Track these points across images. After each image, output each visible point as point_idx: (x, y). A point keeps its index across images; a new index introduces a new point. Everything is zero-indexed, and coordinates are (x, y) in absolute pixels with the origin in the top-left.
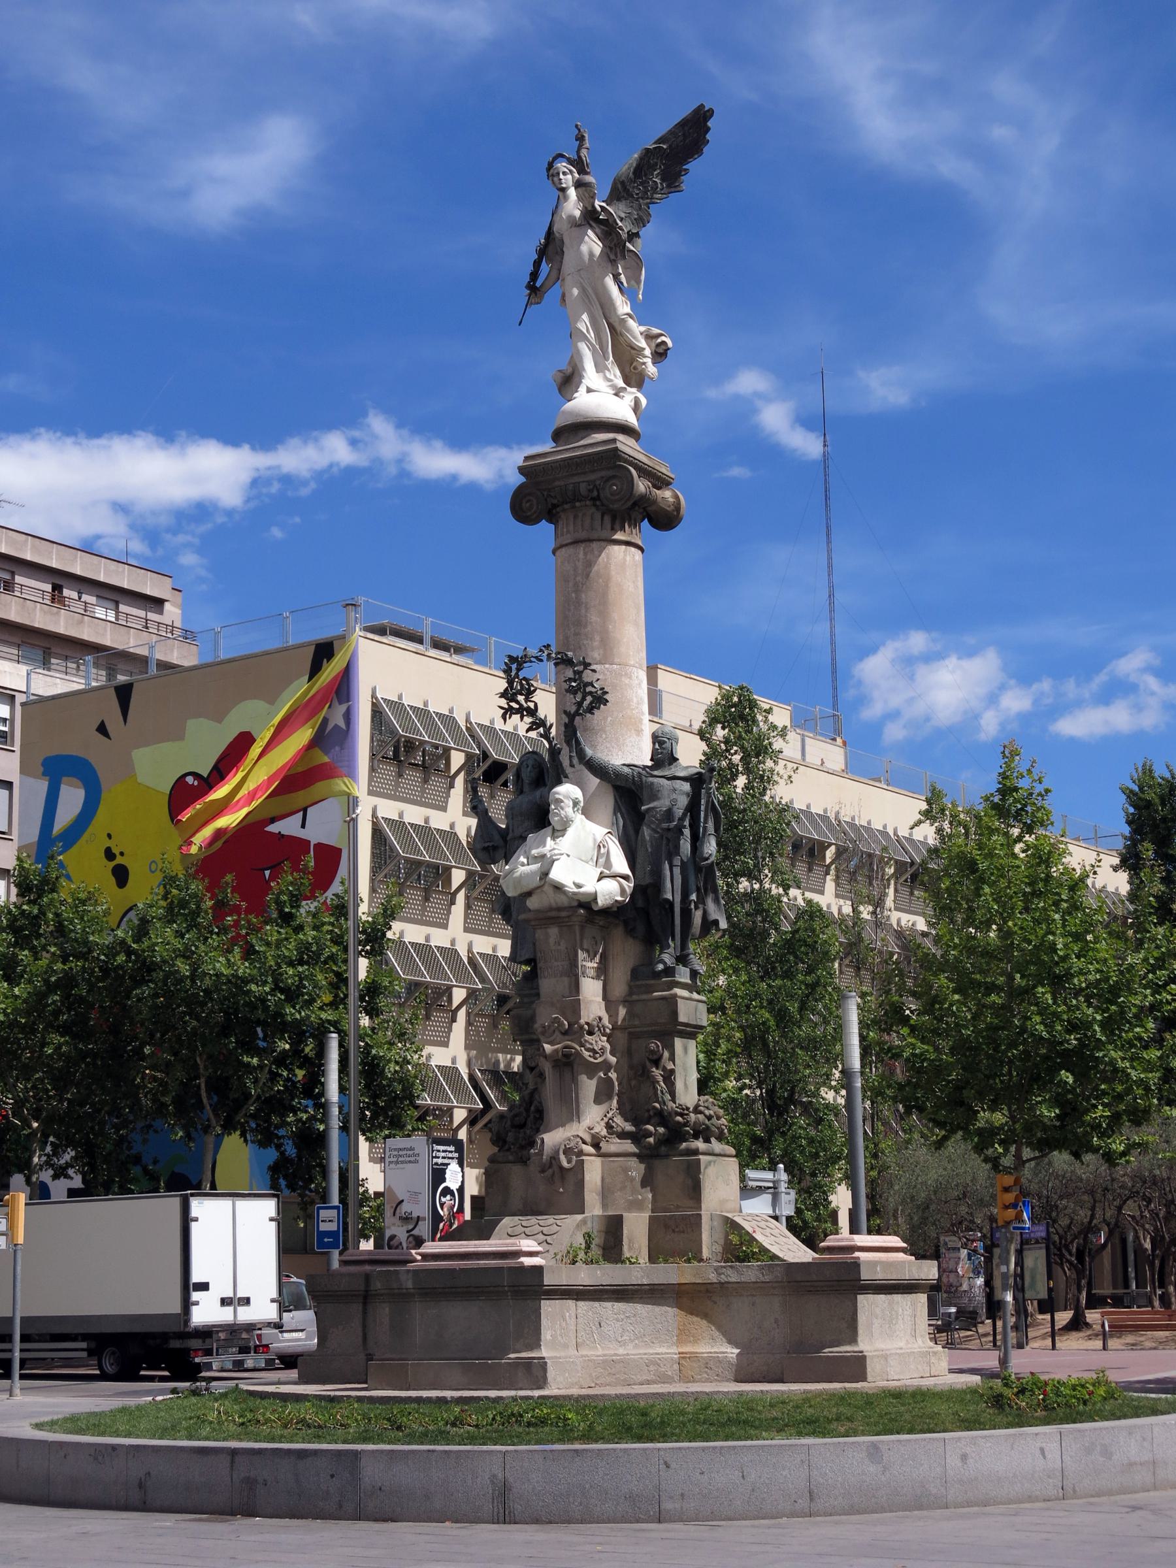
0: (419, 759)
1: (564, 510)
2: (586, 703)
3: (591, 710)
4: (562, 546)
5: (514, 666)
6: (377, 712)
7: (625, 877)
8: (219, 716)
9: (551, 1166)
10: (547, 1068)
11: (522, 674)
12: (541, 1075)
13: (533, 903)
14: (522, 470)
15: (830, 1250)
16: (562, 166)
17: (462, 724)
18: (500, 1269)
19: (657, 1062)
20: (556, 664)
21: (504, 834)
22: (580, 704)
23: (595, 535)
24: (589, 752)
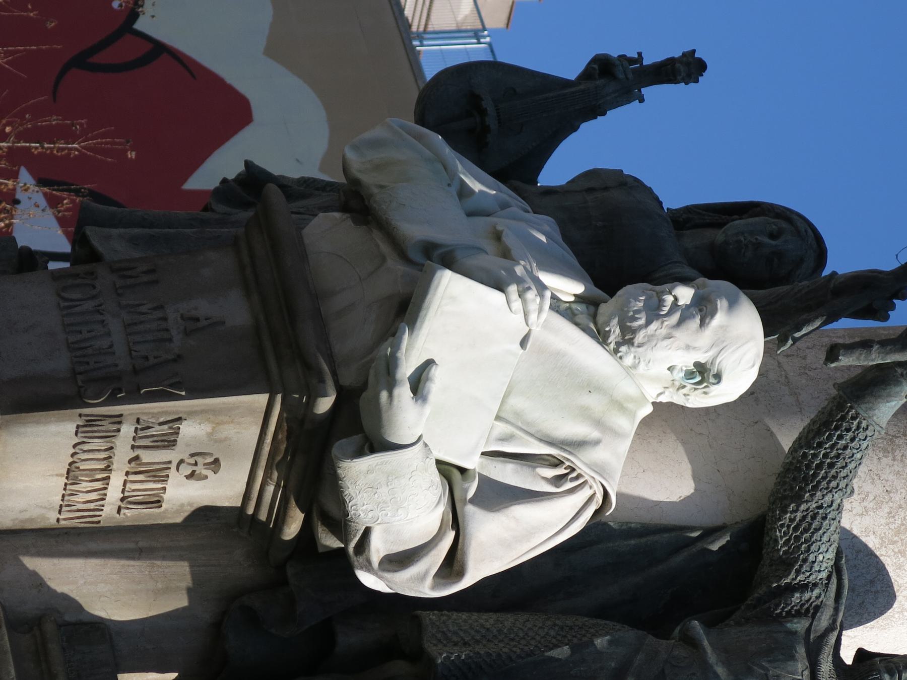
7: (453, 565)
24: (884, 411)
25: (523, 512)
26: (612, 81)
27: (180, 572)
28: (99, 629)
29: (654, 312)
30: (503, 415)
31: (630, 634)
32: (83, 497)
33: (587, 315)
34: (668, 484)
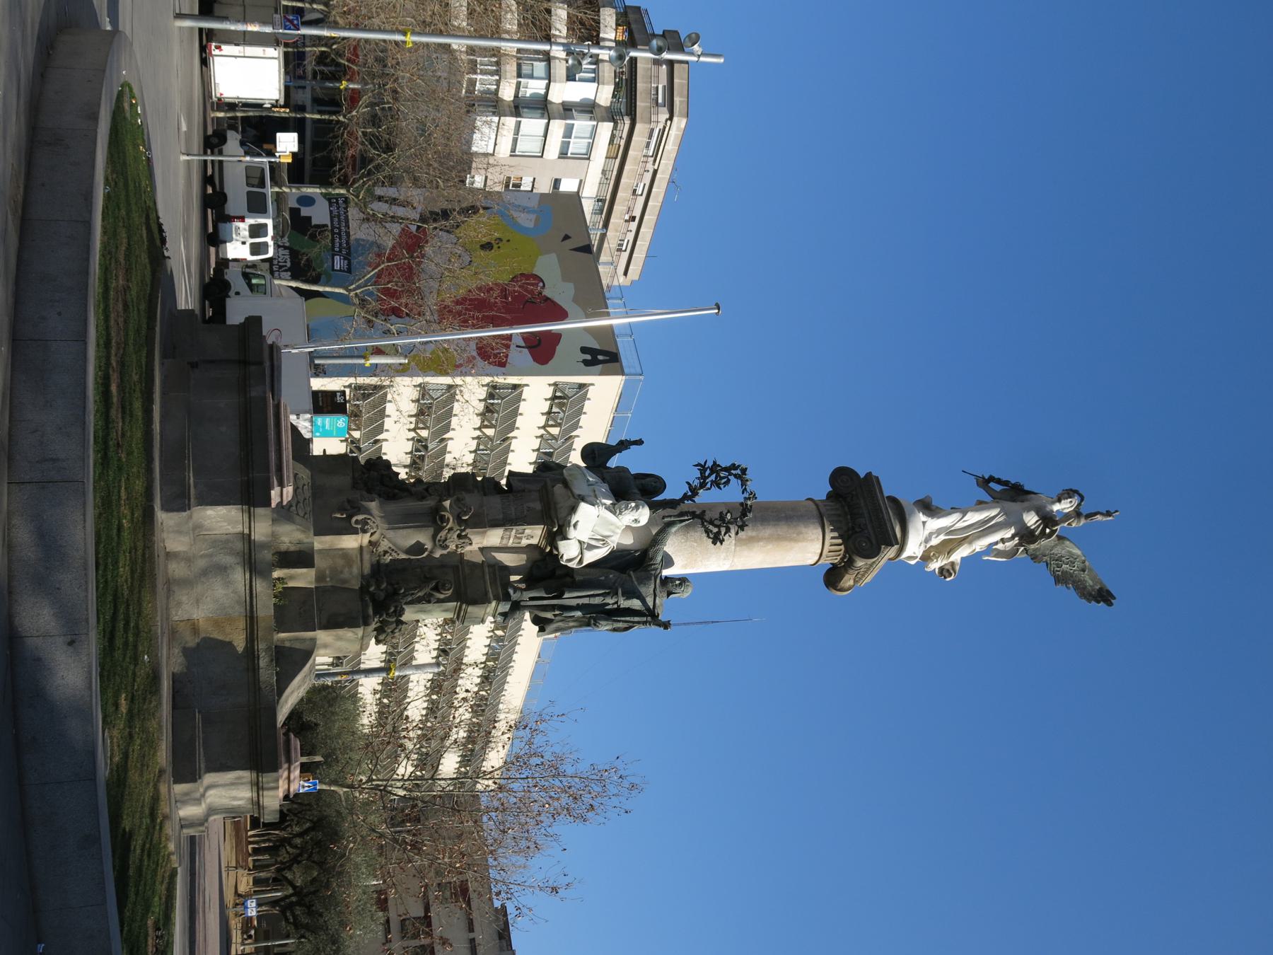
0: (555, 410)
2: (711, 527)
3: (707, 532)
4: (817, 505)
5: (738, 472)
6: (582, 386)
7: (581, 561)
8: (575, 300)
9: (353, 508)
10: (430, 503)
11: (731, 478)
12: (423, 498)
13: (559, 489)
14: (869, 475)
15: (288, 742)
16: (1075, 501)
17: (510, 435)
18: (267, 469)
19: (436, 589)
20: (742, 504)
21: (603, 465)
22: (711, 523)
24: (674, 529)
25: (596, 551)
26: (623, 445)
27: (524, 556)
28: (507, 567)
29: (626, 508)
30: (676, 66)
31: (617, 574)
32: (505, 542)
33: (612, 509)
34: (628, 541)
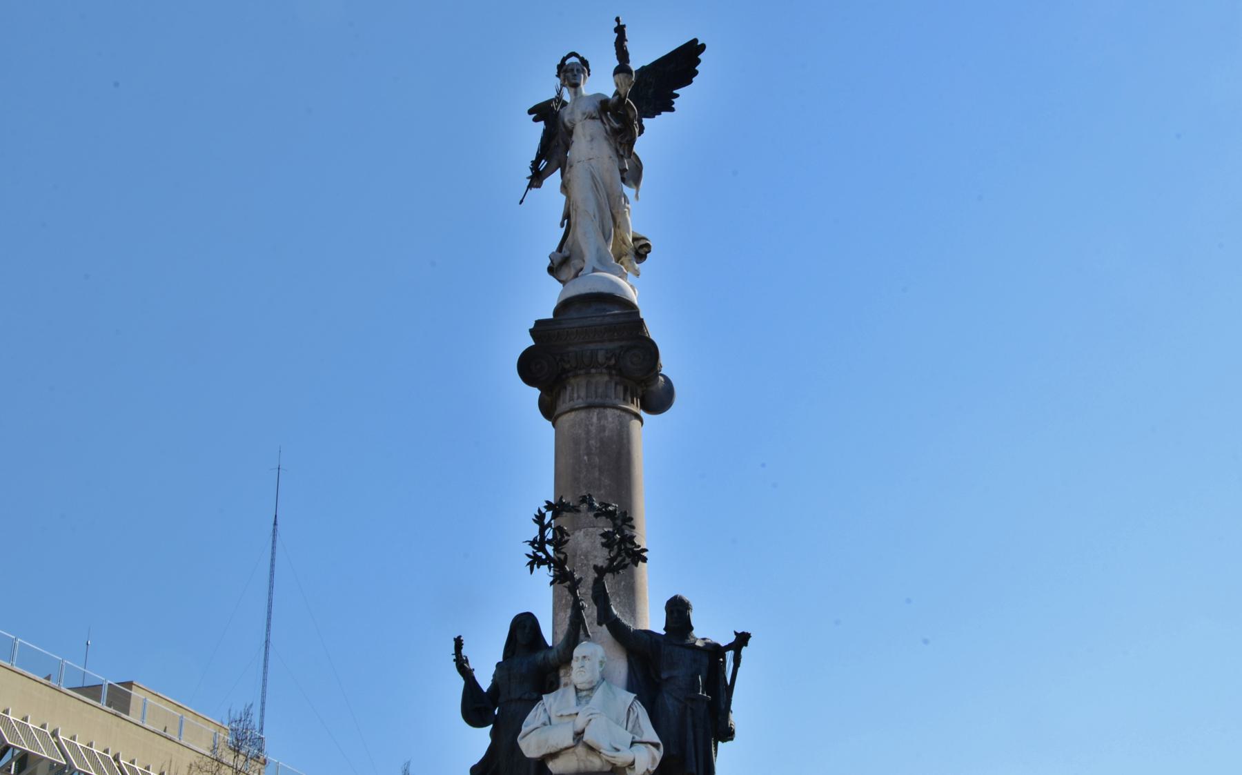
1: (576, 376)
23: (608, 401)
